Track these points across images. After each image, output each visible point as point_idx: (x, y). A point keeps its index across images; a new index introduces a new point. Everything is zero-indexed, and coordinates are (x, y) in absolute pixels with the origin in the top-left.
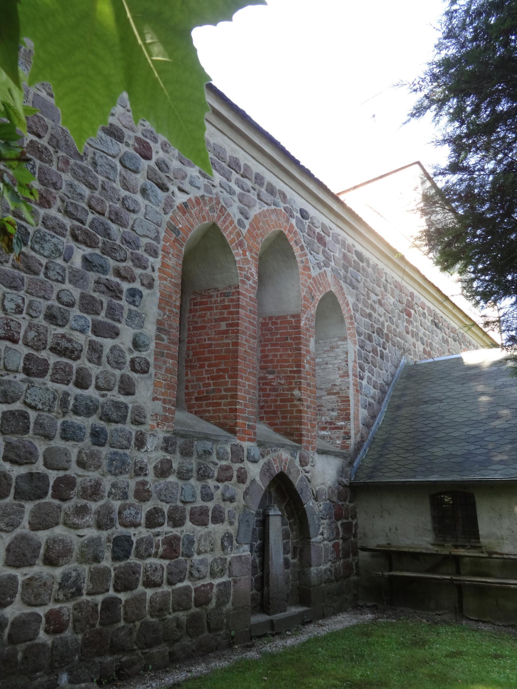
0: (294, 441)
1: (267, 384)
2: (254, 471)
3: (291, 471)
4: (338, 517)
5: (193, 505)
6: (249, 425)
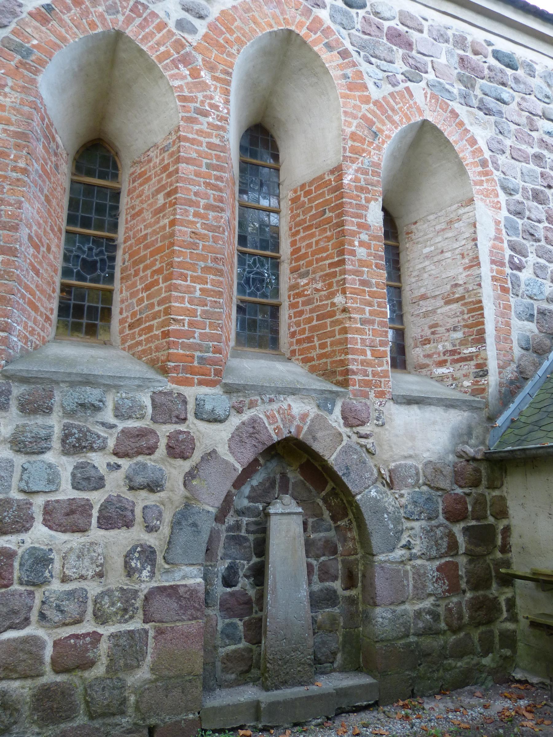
0: (338, 384)
1: (298, 295)
2: (216, 438)
3: (319, 435)
4: (455, 515)
5: (52, 497)
6: (201, 358)
